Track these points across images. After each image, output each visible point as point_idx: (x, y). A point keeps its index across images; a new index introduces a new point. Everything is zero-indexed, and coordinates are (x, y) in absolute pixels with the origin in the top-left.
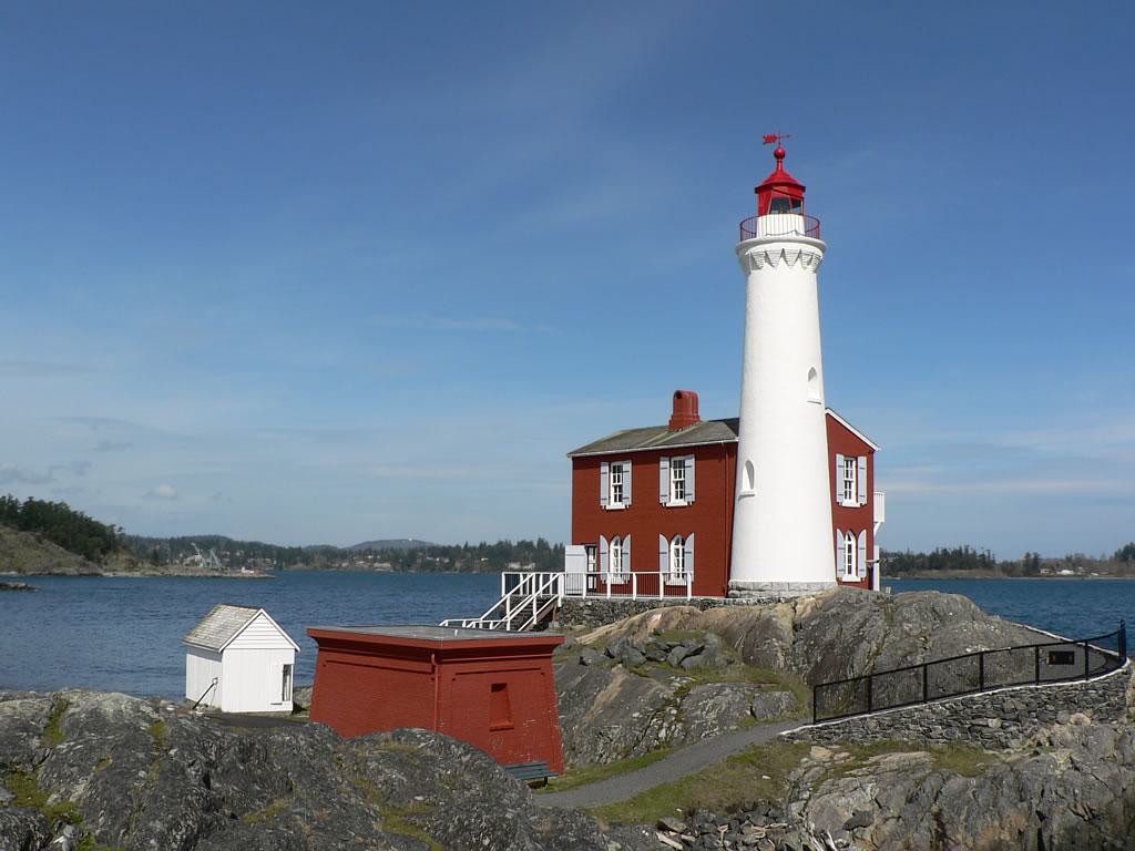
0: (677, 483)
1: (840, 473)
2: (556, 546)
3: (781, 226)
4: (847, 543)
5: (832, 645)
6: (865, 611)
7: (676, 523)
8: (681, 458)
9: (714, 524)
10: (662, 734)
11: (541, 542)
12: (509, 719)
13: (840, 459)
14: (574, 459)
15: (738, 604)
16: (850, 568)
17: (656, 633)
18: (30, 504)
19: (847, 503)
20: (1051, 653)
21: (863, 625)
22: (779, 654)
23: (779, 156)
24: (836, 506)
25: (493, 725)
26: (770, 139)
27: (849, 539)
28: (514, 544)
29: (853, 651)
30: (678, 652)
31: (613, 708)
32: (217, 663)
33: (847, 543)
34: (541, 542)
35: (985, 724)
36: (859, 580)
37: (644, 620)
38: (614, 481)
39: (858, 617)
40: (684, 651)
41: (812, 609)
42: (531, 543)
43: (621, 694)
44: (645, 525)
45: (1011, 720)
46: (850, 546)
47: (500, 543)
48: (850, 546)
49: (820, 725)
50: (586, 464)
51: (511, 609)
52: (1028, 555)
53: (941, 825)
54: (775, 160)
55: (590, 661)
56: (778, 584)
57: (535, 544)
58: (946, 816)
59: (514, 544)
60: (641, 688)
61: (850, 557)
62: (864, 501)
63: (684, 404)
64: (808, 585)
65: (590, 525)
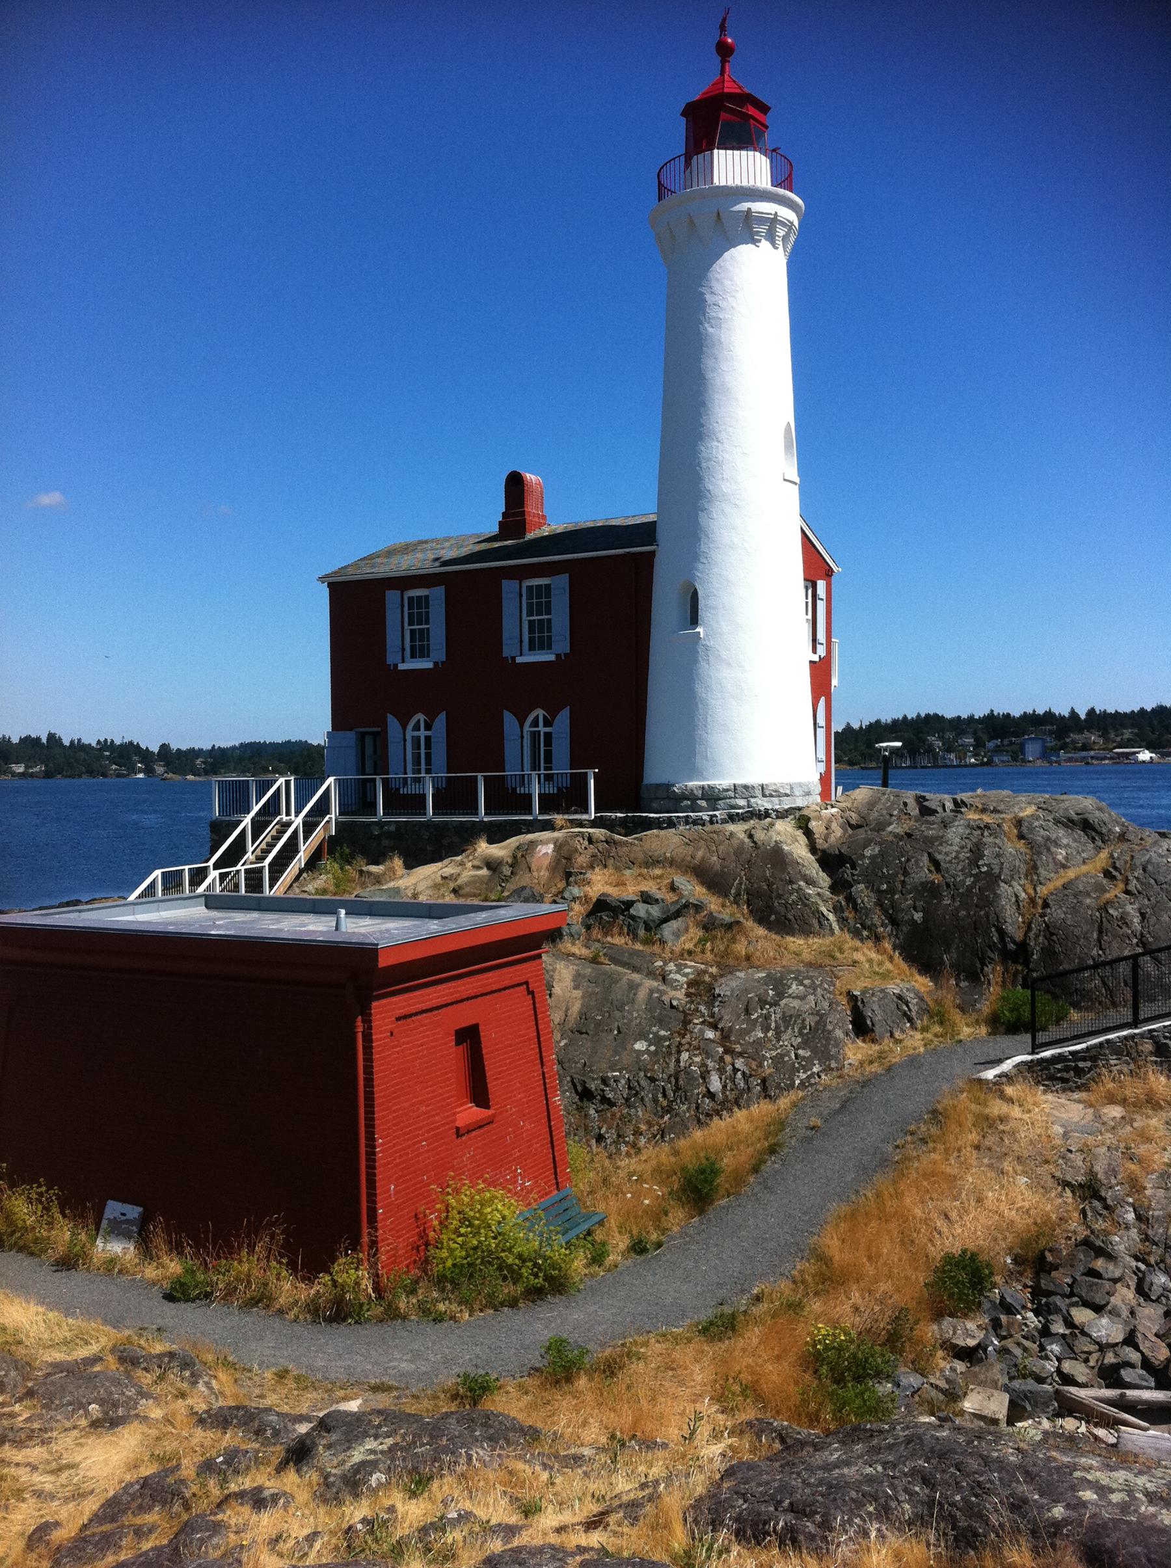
2: (72, 742)
3: (738, 168)
11: (51, 736)
28: (15, 740)
32: (481, 1028)
34: (51, 736)
38: (530, 614)
42: (38, 739)
49: (1047, 1054)
51: (253, 843)
54: (717, 59)
56: (746, 787)
57: (44, 740)
59: (15, 740)
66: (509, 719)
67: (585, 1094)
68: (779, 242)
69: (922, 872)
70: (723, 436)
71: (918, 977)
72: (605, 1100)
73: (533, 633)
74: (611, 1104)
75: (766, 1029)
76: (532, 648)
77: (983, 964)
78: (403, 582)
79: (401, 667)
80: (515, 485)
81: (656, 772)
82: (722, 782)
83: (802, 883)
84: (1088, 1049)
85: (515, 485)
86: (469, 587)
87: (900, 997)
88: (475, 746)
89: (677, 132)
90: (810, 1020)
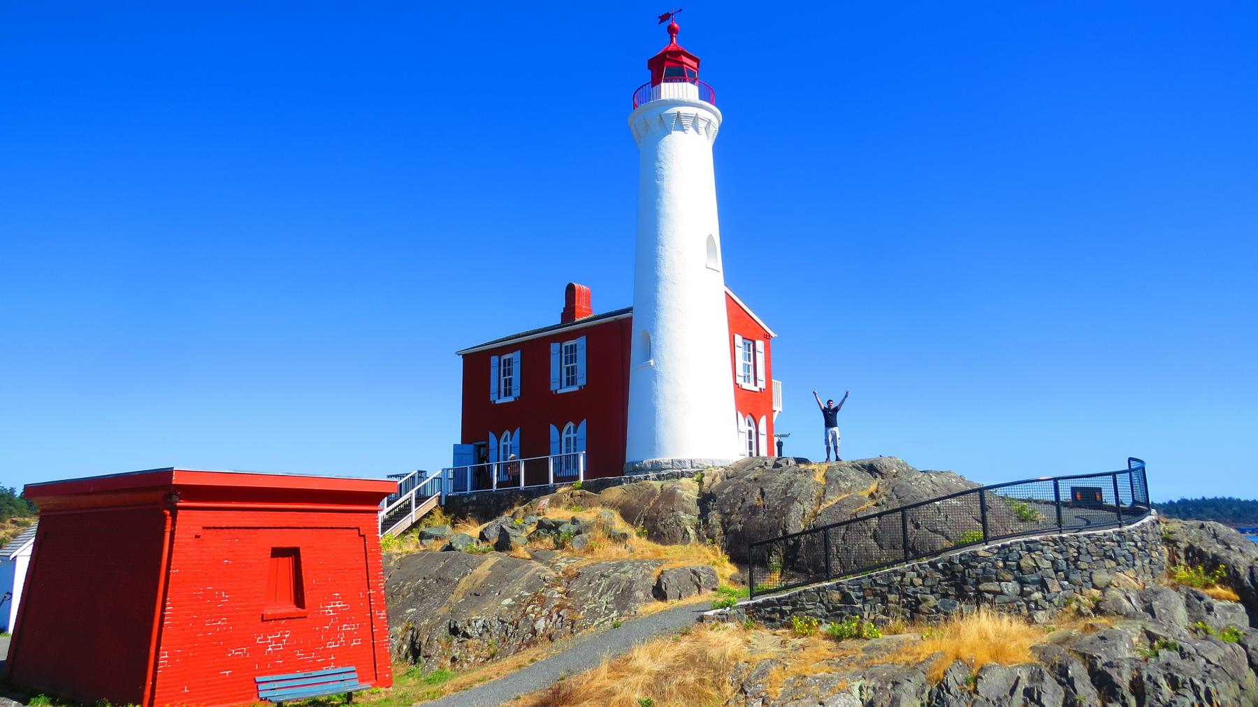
1: (740, 353)
13: (738, 339)
14: (464, 356)
15: (636, 481)
20: (1074, 490)
23: (672, 31)
26: (664, 18)
31: (477, 595)
35: (998, 589)
41: (722, 479)
43: (488, 579)
45: (1034, 583)
46: (750, 432)
49: (760, 600)
55: (460, 547)
56: (680, 461)
62: (762, 384)
66: (553, 430)
67: (454, 631)
68: (702, 131)
69: (755, 499)
70: (665, 242)
71: (727, 564)
72: (466, 635)
73: (567, 374)
74: (468, 637)
75: (595, 592)
76: (568, 384)
77: (770, 555)
78: (501, 350)
79: (498, 402)
80: (570, 289)
81: (631, 455)
82: (664, 459)
83: (681, 513)
84: (790, 597)
85: (570, 289)
86: (534, 350)
87: (694, 572)
88: (535, 446)
89: (647, 76)
90: (623, 584)
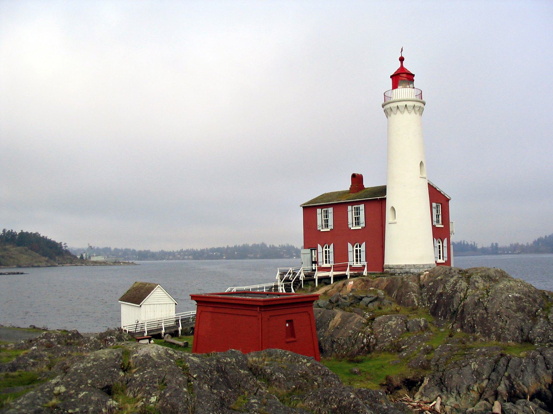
0: (355, 218)
1: (434, 211)
4: (438, 244)
5: (441, 295)
6: (455, 278)
7: (356, 237)
8: (358, 206)
9: (375, 236)
10: (365, 340)
12: (295, 337)
14: (303, 207)
16: (440, 256)
17: (352, 290)
18: (22, 234)
19: (437, 226)
21: (456, 284)
22: (415, 300)
24: (434, 227)
25: (287, 340)
27: (439, 243)
29: (452, 297)
30: (366, 300)
33: (438, 244)
36: (444, 262)
37: (344, 285)
39: (452, 280)
40: (369, 300)
44: (340, 237)
46: (439, 246)
47: (244, 245)
48: (439, 246)
50: (309, 209)
52: (492, 244)
53: (511, 382)
56: (409, 265)
58: (513, 377)
60: (351, 318)
61: (440, 251)
63: (357, 179)
64: (423, 265)
65: (312, 238)
